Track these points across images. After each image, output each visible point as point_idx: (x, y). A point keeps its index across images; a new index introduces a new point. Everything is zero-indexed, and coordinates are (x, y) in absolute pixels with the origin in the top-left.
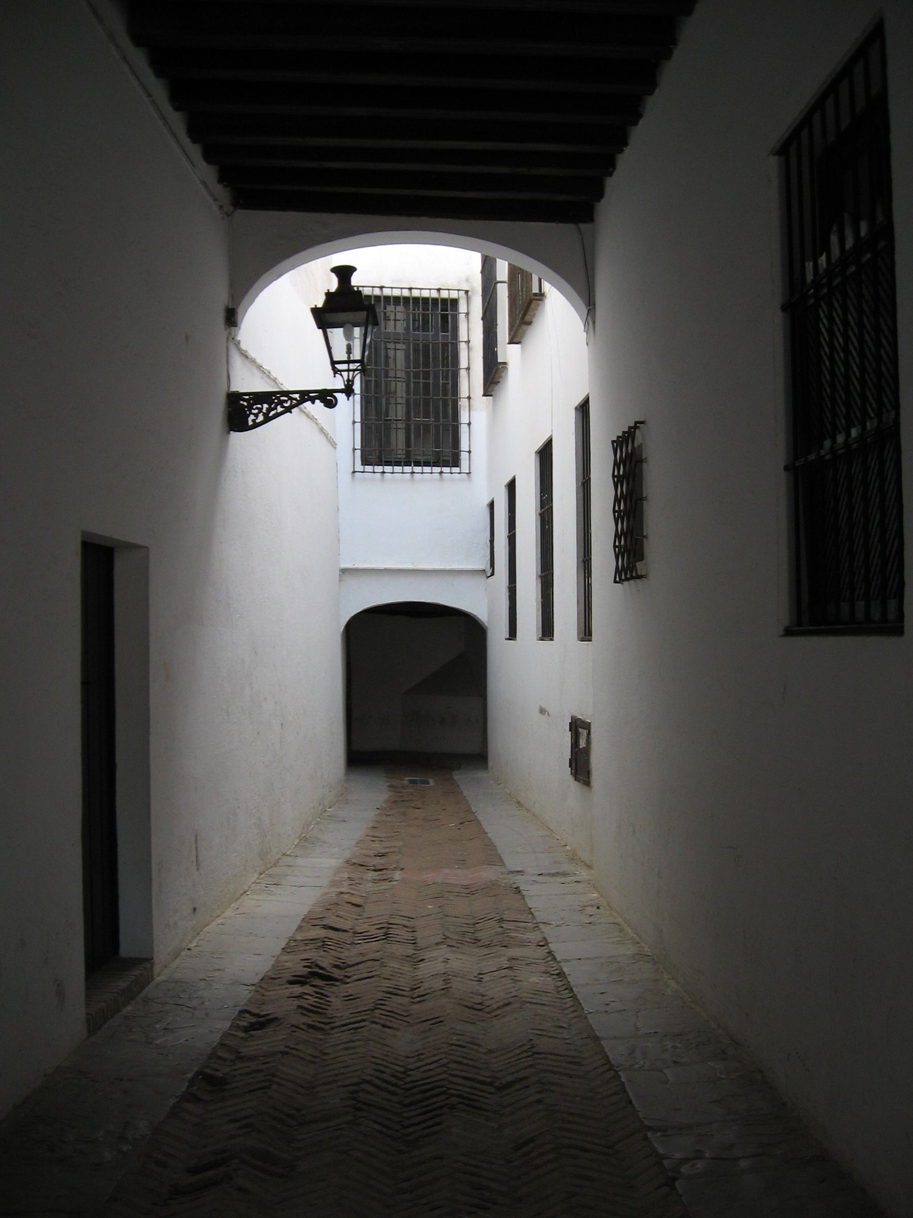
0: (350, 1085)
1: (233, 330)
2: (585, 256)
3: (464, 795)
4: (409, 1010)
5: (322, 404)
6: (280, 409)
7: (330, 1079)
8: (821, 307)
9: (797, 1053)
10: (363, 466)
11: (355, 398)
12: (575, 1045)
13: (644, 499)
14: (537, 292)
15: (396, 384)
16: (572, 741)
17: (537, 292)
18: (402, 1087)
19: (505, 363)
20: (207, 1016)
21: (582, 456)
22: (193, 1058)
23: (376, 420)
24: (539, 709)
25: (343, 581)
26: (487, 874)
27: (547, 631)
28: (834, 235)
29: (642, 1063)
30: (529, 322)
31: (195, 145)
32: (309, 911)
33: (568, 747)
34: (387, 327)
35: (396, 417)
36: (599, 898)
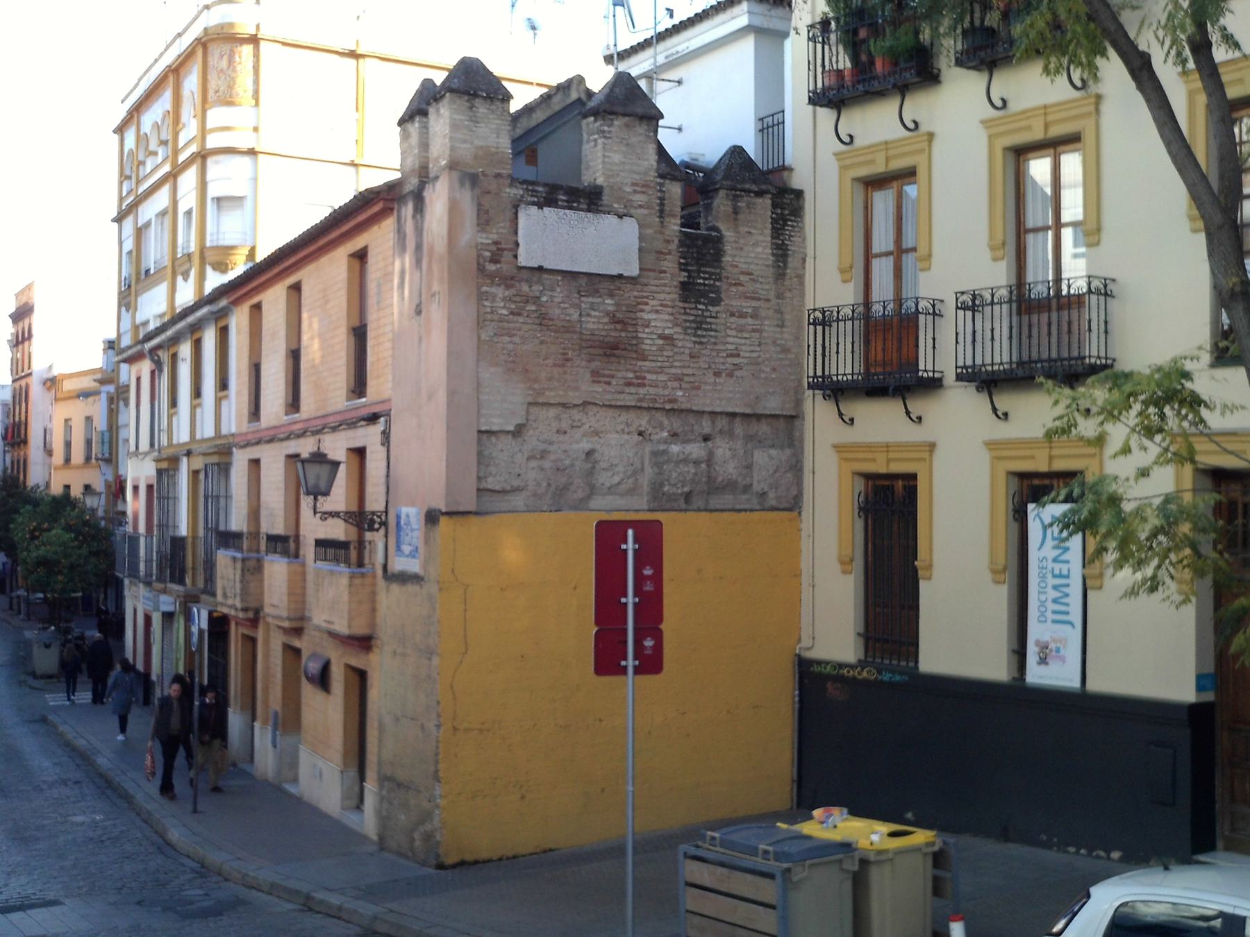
0: (1011, 342)
1: (62, 695)
2: (509, 512)
3: (545, 208)
4: (192, 93)
5: (328, 215)
6: (575, 205)
7: (914, 232)
8: (643, 338)
9: (600, 261)
10: (811, 107)
11: (210, 175)
12: (1220, 446)
13: (882, 289)
14: (818, 327)
15: (1090, 114)
16: (1086, 902)
17: (818, 327)
18: (124, 194)
19: (995, 259)
20: (673, 580)
21: (874, 218)
22: (584, 337)
23: (1049, 311)
24: (1148, 451)
25: (181, 130)
26: (654, 38)
27: (1067, 613)
28: (443, 107)
29: (556, 294)
30: (838, 76)
31: (798, 188)
32: (612, 848)
33: (371, 452)
34: (455, 518)
35: (1048, 228)
36: (1041, 12)
